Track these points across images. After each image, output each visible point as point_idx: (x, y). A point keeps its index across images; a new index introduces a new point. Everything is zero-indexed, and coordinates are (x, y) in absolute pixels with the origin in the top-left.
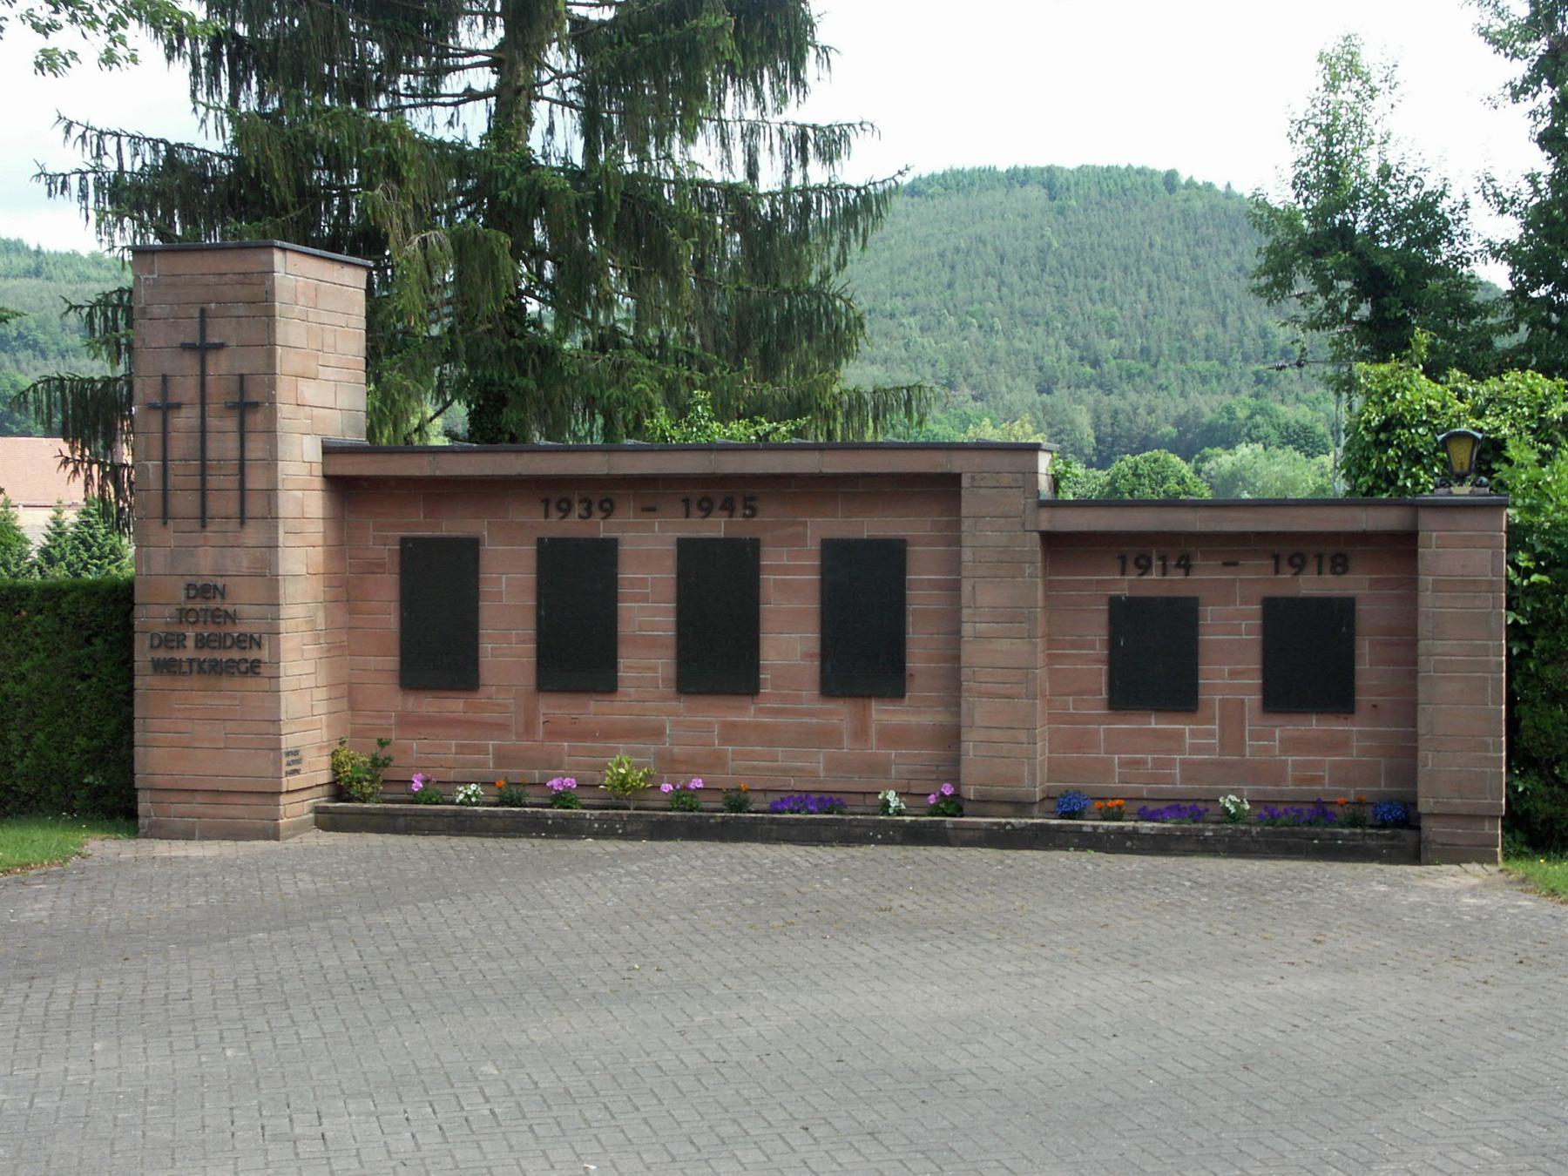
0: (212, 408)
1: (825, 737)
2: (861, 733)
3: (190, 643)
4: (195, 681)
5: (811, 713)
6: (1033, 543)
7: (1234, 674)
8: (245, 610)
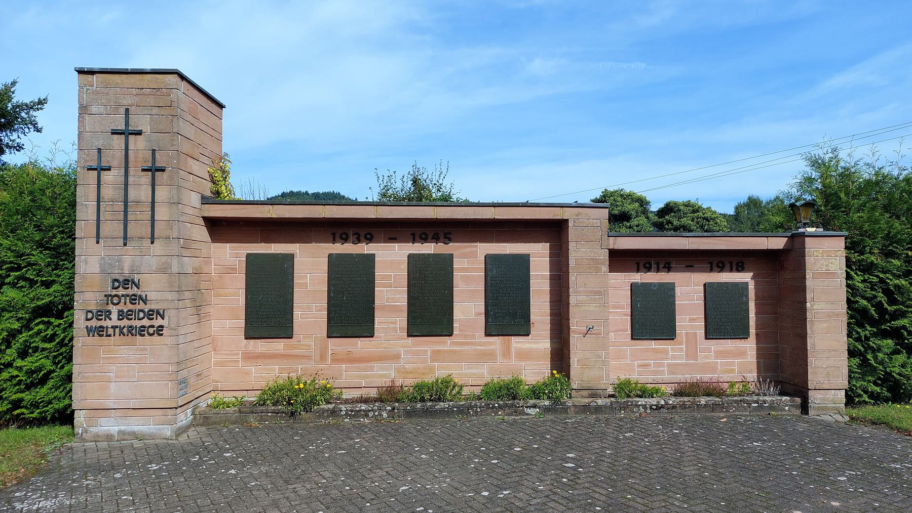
0: (131, 171)
1: (488, 356)
2: (507, 353)
3: (114, 316)
4: (117, 339)
5: (480, 344)
6: (604, 256)
7: (691, 320)
8: (151, 296)
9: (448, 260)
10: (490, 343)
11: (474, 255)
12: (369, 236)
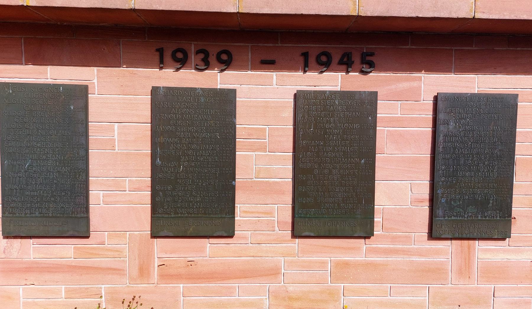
2: (465, 269)
5: (420, 253)
9: (368, 103)
10: (437, 252)
11: (413, 96)
12: (224, 57)
